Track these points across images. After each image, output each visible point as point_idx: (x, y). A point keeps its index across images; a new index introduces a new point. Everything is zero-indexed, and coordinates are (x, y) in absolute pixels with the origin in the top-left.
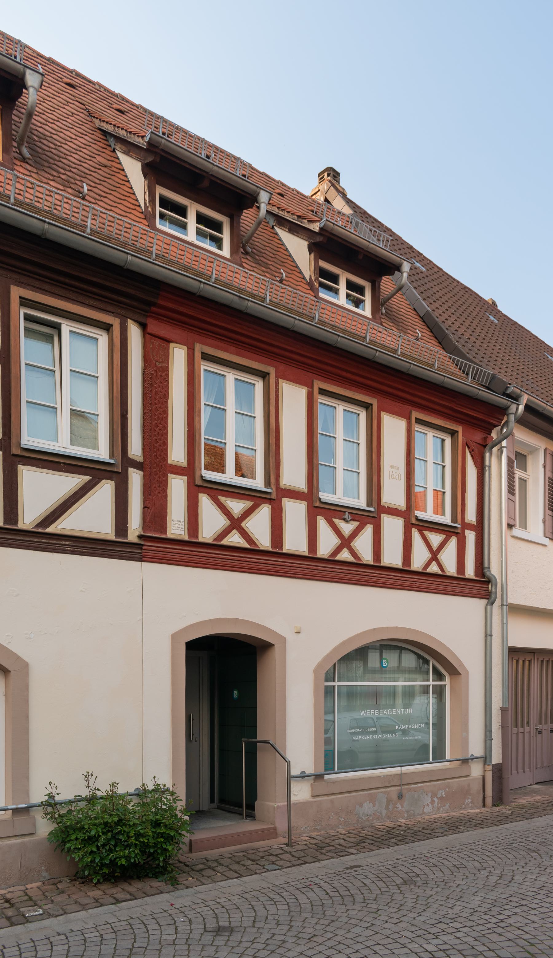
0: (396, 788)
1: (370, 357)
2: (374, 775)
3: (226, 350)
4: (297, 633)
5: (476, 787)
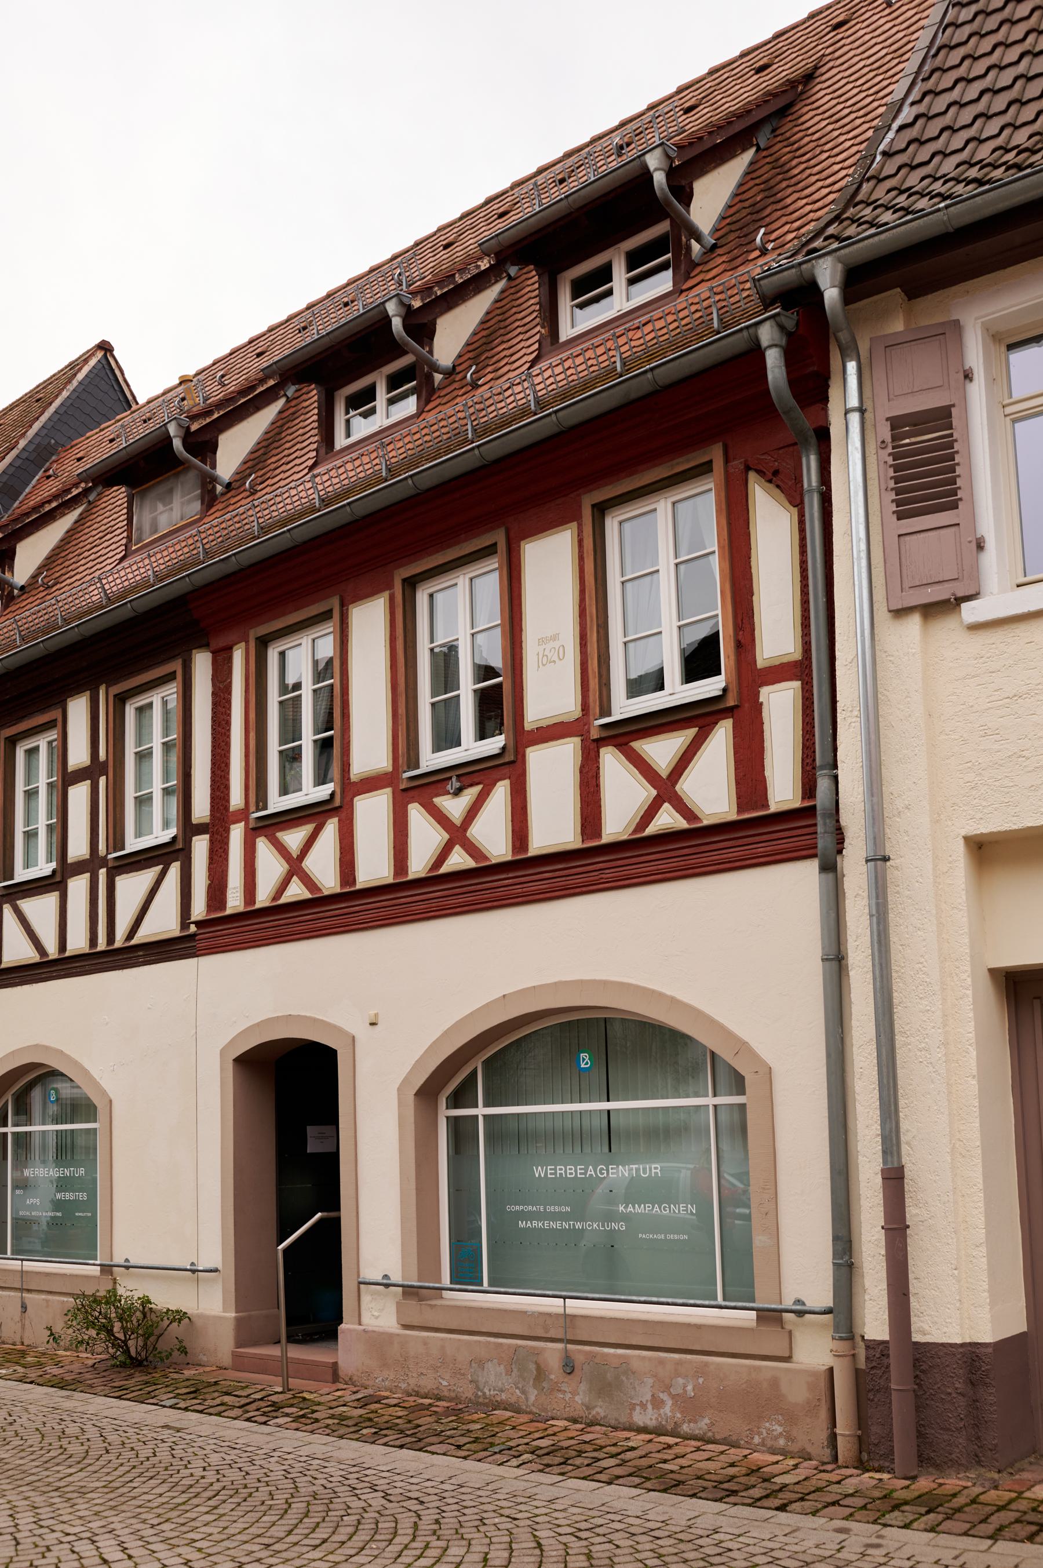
1: (556, 430)
2: (634, 1316)
3: (284, 614)
4: (372, 1024)
5: (797, 1394)
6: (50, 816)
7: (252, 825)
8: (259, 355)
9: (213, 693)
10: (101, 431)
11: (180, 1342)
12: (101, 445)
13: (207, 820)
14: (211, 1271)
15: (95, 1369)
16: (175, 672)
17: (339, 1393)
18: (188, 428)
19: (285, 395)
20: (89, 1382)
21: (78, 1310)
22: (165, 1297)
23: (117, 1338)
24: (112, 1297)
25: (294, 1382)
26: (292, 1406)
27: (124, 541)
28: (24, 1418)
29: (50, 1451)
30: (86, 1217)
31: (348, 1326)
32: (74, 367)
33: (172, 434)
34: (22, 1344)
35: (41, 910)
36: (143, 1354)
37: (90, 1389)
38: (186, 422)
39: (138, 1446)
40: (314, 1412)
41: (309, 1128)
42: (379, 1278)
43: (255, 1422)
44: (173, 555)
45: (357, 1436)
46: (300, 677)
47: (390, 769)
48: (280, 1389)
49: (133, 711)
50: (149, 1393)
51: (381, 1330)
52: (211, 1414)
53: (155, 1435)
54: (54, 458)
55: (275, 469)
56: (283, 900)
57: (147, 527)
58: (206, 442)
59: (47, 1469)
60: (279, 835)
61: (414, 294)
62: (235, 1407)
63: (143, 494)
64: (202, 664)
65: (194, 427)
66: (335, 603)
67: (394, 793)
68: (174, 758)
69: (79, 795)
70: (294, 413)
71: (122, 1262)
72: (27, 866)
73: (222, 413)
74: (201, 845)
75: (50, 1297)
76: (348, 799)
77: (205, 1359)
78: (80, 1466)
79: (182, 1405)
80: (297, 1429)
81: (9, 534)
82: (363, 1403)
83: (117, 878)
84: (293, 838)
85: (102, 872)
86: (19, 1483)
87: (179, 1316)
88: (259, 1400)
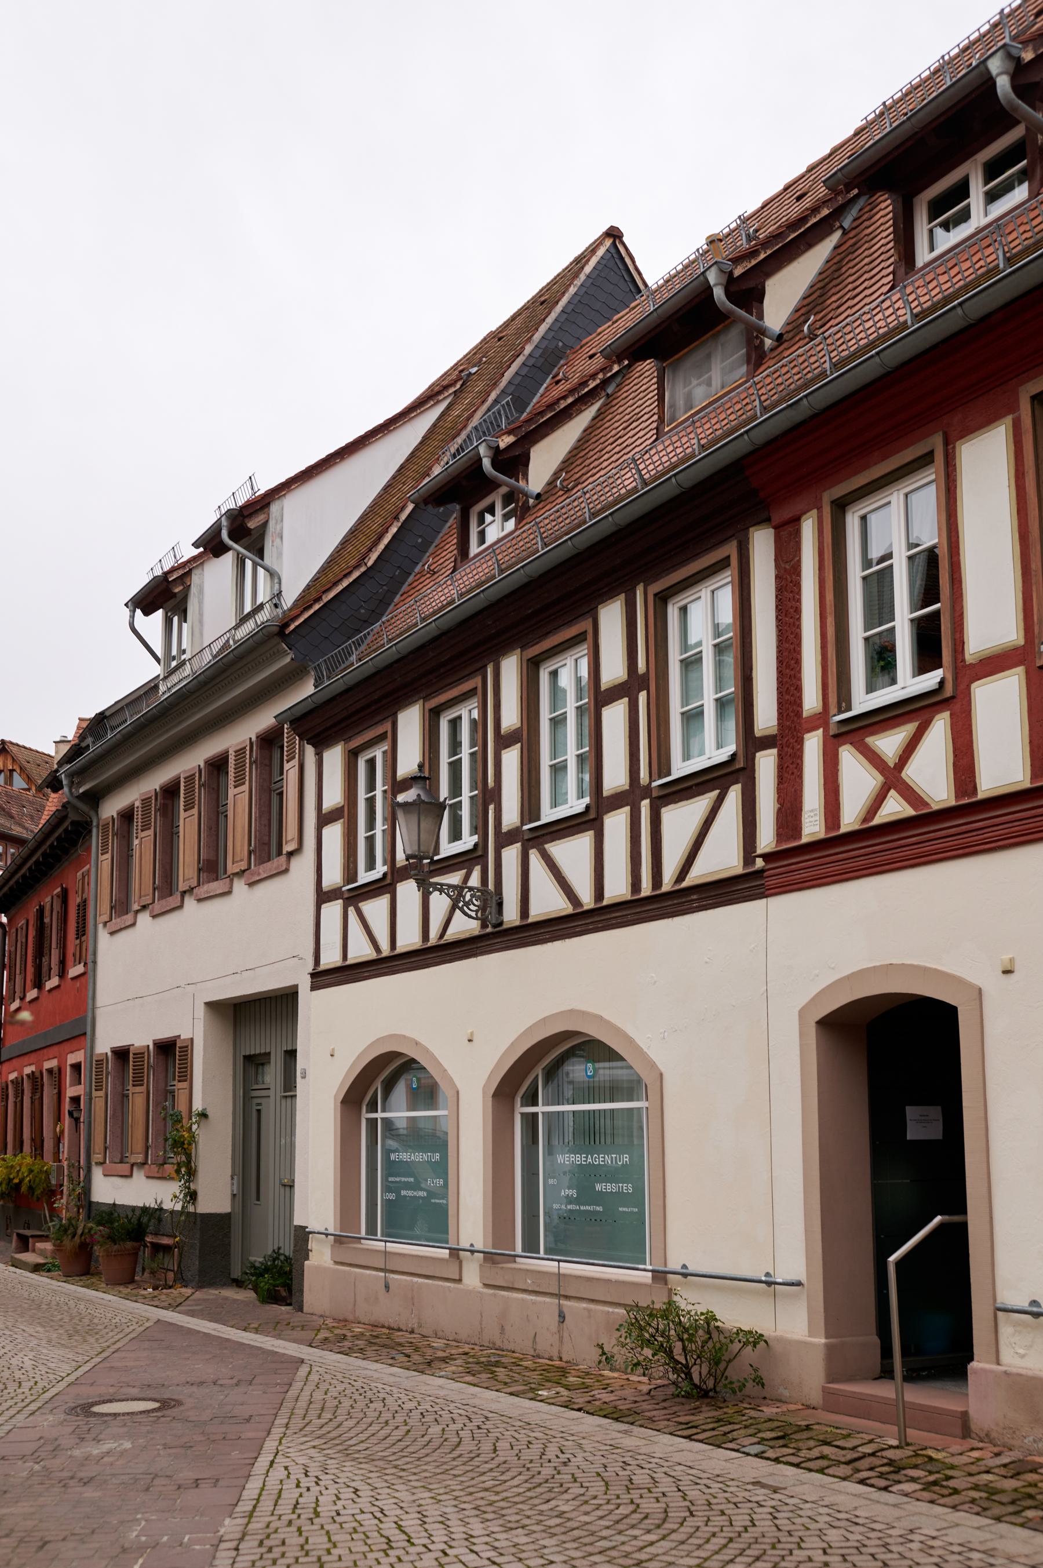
6: (580, 745)
7: (833, 730)
8: (798, 199)
9: (777, 577)
10: (614, 323)
11: (756, 1370)
12: (626, 321)
13: (774, 731)
14: (792, 1284)
15: (653, 1397)
16: (729, 557)
17: (975, 1454)
18: (731, 273)
19: (841, 227)
20: (648, 1414)
21: (632, 1325)
22: (735, 1314)
23: (678, 1362)
24: (670, 1310)
25: (912, 1434)
26: (915, 1467)
27: (655, 425)
28: (579, 1459)
29: (618, 1506)
30: (632, 1212)
31: (981, 1365)
32: (580, 261)
33: (712, 283)
34: (561, 1359)
35: (573, 853)
36: (710, 1383)
37: (650, 1423)
38: (728, 266)
39: (730, 1510)
40: (949, 1478)
41: (907, 1108)
42: (1024, 1304)
43: (872, 1486)
44: (717, 426)
45: (1020, 1520)
46: (891, 545)
47: (1022, 642)
48: (894, 1442)
49: (676, 612)
50: (725, 1434)
51: (1030, 1373)
52: (810, 1470)
53: (747, 1494)
54: (562, 362)
55: (838, 307)
56: (877, 821)
57: (681, 403)
58: (751, 290)
59: (620, 1533)
60: (869, 740)
61: (1025, 43)
62: (840, 1462)
63: (675, 366)
64: (762, 544)
65: (738, 271)
66: (936, 442)
67: (1027, 673)
68: (730, 659)
69: (615, 716)
70: (855, 244)
71: (678, 1268)
72: (554, 804)
73: (769, 252)
74: (766, 763)
75: (592, 1306)
76: (962, 687)
77: (786, 1393)
78: (661, 1532)
79: (771, 1454)
80: (932, 1502)
81: (522, 437)
82: (1017, 1469)
83: (663, 810)
84: (889, 744)
85: (645, 804)
86: (589, 1549)
87: (755, 1339)
88: (870, 1455)
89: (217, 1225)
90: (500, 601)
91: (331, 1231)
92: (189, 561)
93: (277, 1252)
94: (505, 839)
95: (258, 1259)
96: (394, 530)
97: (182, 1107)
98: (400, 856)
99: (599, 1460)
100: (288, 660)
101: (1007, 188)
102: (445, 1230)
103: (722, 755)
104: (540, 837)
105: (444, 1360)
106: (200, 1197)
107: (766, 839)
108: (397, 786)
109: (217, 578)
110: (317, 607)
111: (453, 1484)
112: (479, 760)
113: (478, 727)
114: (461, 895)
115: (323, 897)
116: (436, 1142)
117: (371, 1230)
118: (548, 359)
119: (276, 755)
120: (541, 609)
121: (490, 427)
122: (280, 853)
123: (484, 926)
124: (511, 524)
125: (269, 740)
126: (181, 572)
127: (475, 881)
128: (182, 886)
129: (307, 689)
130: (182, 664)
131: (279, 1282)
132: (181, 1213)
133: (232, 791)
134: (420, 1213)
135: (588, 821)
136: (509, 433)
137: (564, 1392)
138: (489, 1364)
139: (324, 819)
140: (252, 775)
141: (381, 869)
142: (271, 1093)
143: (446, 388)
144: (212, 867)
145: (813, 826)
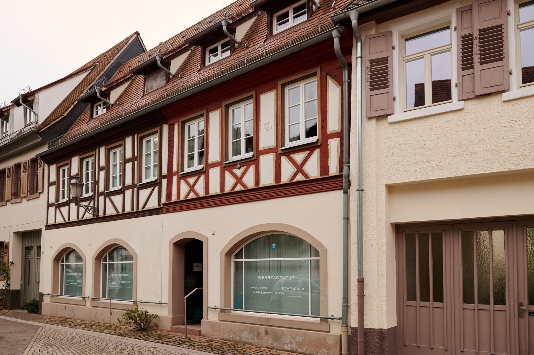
0: (264, 327)
5: (331, 342)
7: (179, 176)
12: (135, 63)
22: (152, 311)
24: (136, 311)
25: (188, 336)
32: (128, 39)
35: (117, 199)
37: (130, 336)
42: (213, 307)
57: (149, 88)
61: (230, 19)
63: (148, 78)
64: (166, 128)
65: (164, 58)
69: (129, 166)
72: (113, 186)
74: (164, 182)
79: (156, 341)
82: (208, 341)
84: (191, 180)
85: (136, 189)
87: (156, 316)
89: (16, 294)
90: (100, 133)
91: (50, 293)
92: (9, 106)
93: (34, 300)
94: (100, 194)
95: (28, 302)
96: (72, 107)
97: (5, 260)
98: (71, 196)
99: (115, 344)
100: (40, 140)
101: (226, 51)
102: (82, 293)
103: (154, 179)
104: (109, 194)
105: (80, 325)
106: (11, 285)
107: (164, 200)
108: (71, 178)
109: (18, 113)
110: (49, 126)
111: (78, 351)
112: (94, 173)
113: (94, 164)
114: (88, 208)
115: (49, 205)
116: (79, 270)
117: (62, 293)
118: (118, 65)
119: (36, 165)
120: (111, 136)
121: (99, 85)
122: (37, 192)
123: (94, 216)
124: (105, 110)
125: (34, 161)
126: (6, 109)
127: (92, 204)
128: (6, 199)
129: (45, 149)
130: (7, 136)
131: (35, 308)
132: (5, 290)
133: (22, 174)
134: (73, 288)
135: (121, 192)
136: (105, 87)
137: (110, 331)
138: (91, 325)
139: (50, 184)
140: (28, 170)
141: (66, 199)
142: (33, 257)
143: (89, 67)
144: (16, 194)
145: (174, 198)
